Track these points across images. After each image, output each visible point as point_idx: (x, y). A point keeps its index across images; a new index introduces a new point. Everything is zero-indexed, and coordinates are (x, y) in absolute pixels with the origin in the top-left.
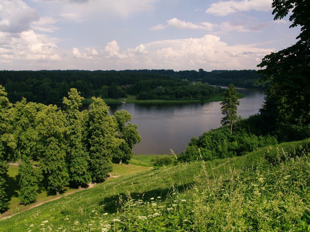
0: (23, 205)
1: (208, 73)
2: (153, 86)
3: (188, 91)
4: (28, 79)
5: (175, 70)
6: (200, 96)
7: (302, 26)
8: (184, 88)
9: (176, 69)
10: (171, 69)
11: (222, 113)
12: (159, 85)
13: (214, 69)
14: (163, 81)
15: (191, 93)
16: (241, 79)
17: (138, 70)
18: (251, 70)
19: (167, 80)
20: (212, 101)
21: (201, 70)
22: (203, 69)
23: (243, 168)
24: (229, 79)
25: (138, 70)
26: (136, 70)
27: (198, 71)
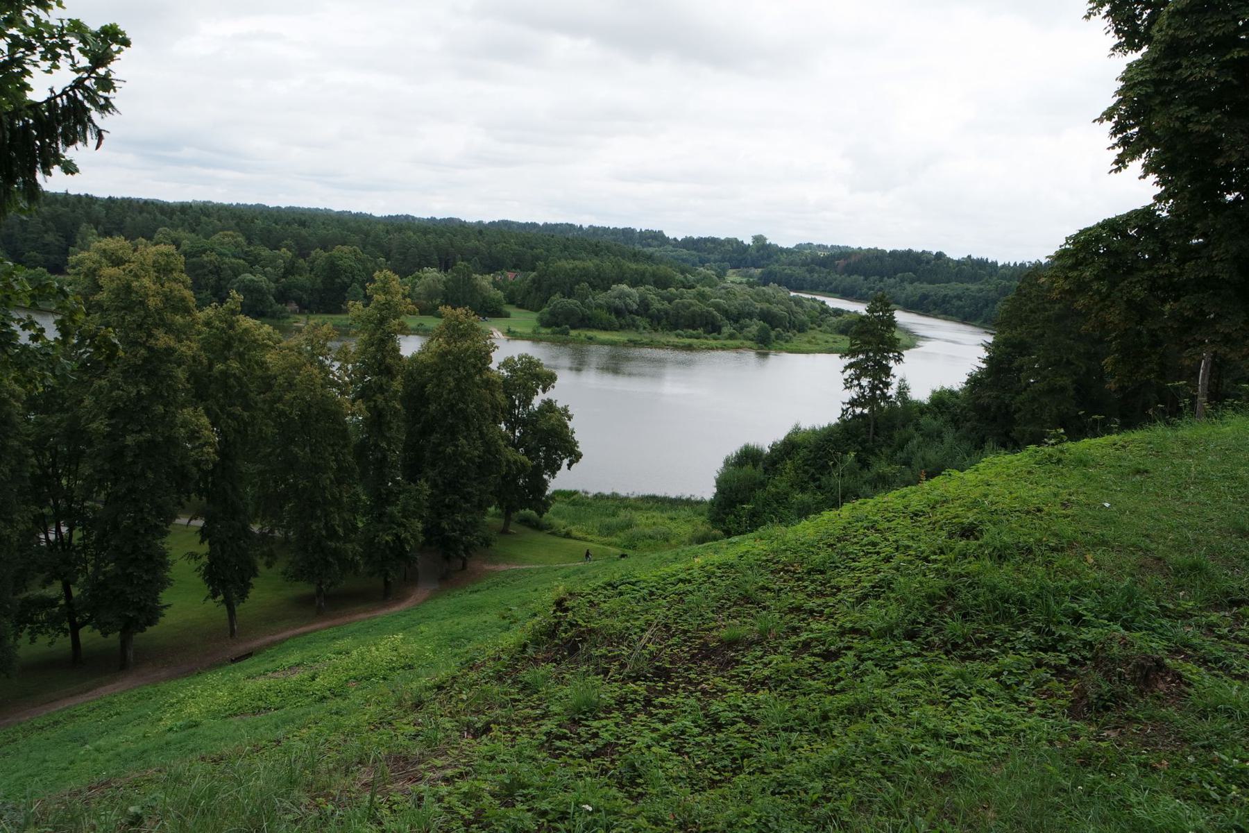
0: (574, 465)
1: (782, 250)
2: (602, 282)
3: (718, 307)
4: (160, 229)
5: (670, 234)
6: (755, 327)
7: (549, 406)
8: (702, 296)
9: (675, 231)
10: (656, 228)
11: (846, 388)
12: (620, 281)
13: (804, 241)
14: (634, 266)
15: (726, 313)
16: (892, 280)
17: (541, 224)
18: (930, 253)
19: (646, 266)
20: (781, 350)
21: (759, 239)
22: (765, 236)
23: (284, 742)
24: (855, 277)
25: (541, 224)
26: (534, 225)
27: (748, 241)
